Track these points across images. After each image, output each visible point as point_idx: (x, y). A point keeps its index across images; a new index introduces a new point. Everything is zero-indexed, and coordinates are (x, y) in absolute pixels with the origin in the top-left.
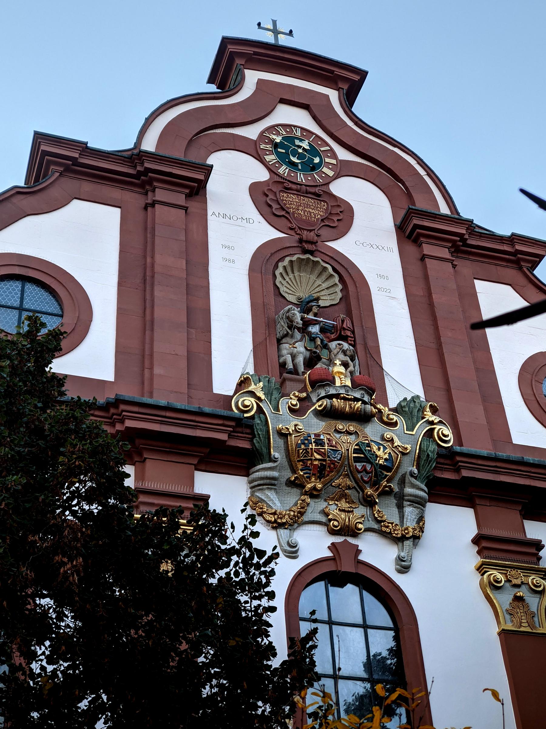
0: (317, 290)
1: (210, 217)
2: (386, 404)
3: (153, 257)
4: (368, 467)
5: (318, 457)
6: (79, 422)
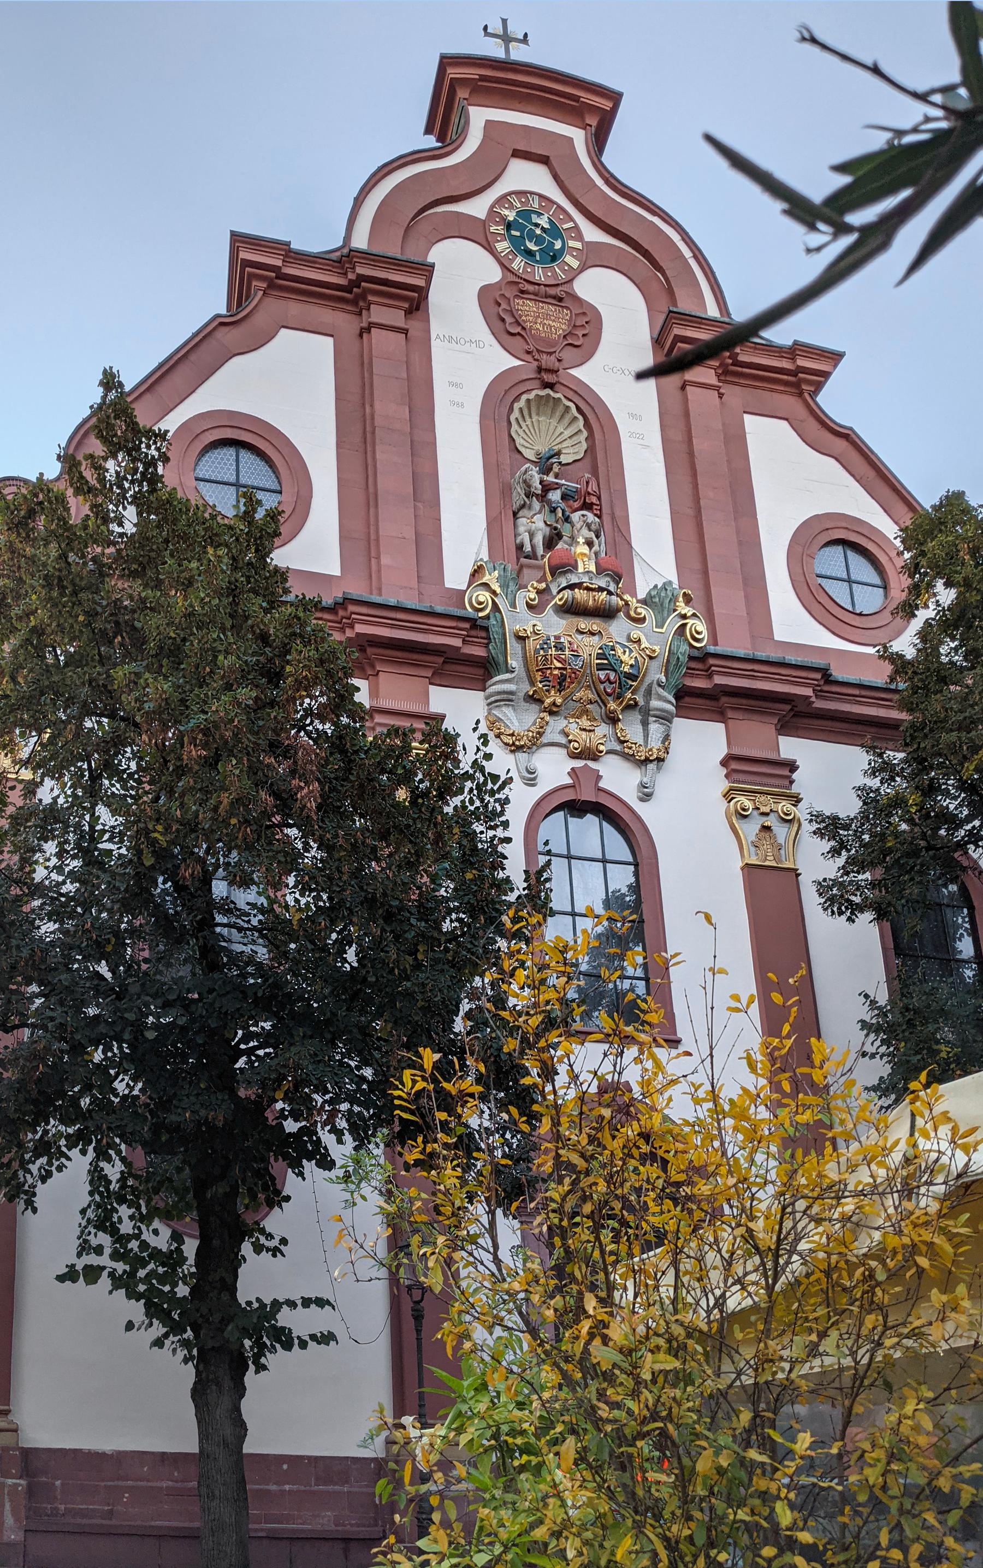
0: (558, 440)
1: (435, 345)
2: (634, 594)
3: (372, 406)
4: (612, 676)
5: (559, 665)
6: (303, 624)
